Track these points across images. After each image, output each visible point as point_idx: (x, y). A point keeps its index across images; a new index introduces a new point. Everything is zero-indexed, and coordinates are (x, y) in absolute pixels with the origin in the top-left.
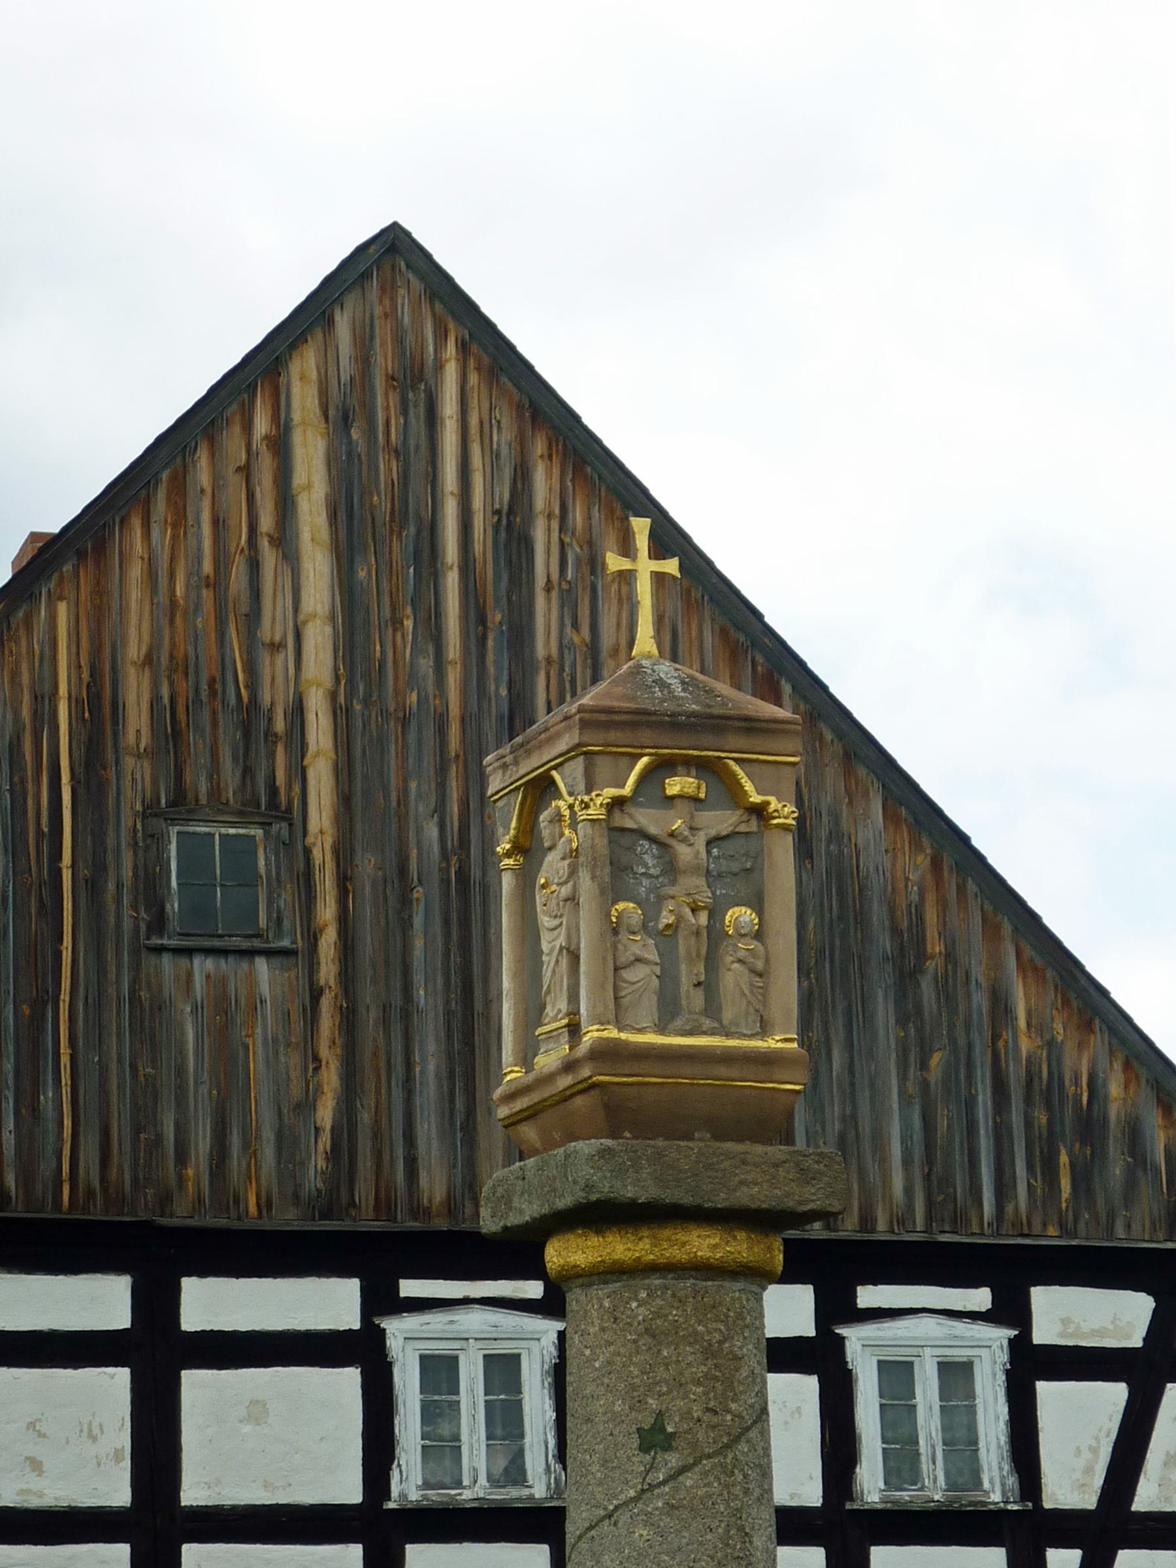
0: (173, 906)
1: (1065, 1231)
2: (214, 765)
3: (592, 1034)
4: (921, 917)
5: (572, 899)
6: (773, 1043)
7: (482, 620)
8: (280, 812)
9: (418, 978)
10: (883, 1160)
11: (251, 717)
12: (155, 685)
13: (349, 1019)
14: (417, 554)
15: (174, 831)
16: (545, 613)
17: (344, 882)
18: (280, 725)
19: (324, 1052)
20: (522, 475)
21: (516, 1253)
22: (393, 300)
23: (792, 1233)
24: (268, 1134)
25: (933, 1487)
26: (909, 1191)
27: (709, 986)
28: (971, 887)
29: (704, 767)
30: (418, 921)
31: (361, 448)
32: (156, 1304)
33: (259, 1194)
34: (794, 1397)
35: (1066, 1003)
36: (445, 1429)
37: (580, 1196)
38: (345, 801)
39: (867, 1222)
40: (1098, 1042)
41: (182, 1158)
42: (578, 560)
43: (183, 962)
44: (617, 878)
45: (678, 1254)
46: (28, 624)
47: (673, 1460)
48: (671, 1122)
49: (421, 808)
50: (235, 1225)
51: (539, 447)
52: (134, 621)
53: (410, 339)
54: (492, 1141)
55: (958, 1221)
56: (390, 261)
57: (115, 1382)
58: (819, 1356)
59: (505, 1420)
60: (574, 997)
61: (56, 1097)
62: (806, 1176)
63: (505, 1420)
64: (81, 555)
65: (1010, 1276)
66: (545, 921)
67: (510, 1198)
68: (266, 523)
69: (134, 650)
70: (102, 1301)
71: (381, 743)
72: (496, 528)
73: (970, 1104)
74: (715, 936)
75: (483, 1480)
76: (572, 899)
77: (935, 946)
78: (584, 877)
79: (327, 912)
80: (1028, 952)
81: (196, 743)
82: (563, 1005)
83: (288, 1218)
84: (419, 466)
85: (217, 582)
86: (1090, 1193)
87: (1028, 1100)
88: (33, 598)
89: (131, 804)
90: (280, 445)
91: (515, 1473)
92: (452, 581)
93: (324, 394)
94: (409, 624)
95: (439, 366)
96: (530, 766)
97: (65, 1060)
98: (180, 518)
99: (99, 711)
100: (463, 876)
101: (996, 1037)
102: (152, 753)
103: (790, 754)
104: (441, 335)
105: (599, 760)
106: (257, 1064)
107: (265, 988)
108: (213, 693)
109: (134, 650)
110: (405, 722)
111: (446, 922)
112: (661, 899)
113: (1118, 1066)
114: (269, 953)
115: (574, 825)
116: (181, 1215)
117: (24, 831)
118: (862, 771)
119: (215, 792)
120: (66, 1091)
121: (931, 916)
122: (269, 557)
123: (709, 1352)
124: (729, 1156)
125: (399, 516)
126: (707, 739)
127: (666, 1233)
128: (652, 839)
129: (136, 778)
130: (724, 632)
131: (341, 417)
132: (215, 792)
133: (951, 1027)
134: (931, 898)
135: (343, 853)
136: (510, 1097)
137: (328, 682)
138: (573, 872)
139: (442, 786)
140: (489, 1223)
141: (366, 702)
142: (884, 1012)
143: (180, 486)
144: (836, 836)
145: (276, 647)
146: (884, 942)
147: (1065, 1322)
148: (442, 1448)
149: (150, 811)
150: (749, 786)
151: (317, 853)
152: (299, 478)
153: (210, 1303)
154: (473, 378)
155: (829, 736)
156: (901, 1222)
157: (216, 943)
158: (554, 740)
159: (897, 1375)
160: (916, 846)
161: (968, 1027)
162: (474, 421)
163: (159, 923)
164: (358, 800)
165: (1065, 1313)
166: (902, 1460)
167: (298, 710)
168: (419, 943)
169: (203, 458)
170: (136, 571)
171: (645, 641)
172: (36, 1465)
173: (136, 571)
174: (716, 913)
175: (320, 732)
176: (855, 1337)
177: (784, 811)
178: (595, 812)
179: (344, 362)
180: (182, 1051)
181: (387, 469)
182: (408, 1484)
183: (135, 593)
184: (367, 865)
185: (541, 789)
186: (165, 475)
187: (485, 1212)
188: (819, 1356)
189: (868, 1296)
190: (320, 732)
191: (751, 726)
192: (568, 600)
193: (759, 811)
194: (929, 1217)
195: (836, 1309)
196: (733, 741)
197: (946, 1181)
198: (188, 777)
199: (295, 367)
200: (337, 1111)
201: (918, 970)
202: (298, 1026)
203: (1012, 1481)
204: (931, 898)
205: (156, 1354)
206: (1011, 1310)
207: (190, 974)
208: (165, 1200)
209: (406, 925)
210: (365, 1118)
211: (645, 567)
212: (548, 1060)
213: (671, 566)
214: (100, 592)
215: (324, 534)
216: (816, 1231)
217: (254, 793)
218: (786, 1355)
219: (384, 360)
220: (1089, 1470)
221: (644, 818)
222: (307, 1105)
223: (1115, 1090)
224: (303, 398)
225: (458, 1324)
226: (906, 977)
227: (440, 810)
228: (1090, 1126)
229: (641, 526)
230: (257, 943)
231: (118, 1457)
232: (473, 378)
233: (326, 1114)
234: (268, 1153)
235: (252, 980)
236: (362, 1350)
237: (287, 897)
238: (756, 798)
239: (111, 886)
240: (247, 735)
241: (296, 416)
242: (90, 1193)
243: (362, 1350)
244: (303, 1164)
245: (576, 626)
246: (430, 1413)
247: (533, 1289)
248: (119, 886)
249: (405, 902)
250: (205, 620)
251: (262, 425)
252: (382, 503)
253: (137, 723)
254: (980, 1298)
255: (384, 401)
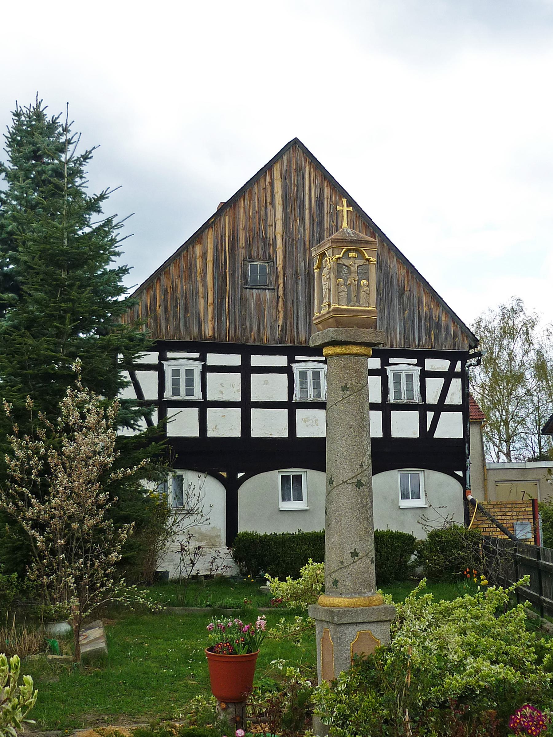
0: (249, 279)
1: (432, 348)
2: (258, 250)
3: (333, 306)
4: (404, 282)
5: (329, 278)
6: (370, 308)
7: (314, 220)
8: (271, 260)
9: (300, 294)
10: (395, 333)
11: (265, 240)
12: (246, 234)
13: (285, 303)
14: (300, 206)
15: (249, 264)
16: (326, 219)
17: (284, 274)
18: (271, 242)
19: (280, 310)
20: (322, 190)
21: (317, 351)
22: (295, 154)
23: (373, 348)
24: (269, 327)
25: (404, 399)
26: (400, 339)
27: (357, 296)
28: (414, 276)
29: (357, 251)
30: (300, 283)
31: (289, 184)
32: (246, 360)
33: (267, 339)
34: (375, 382)
35: (434, 300)
36: (304, 387)
37: (330, 340)
38: (285, 257)
39: (392, 345)
40: (440, 308)
41: (251, 331)
42: (333, 207)
43: (251, 290)
44: (338, 275)
45: (350, 351)
46: (220, 220)
47: (349, 393)
48: (348, 324)
49: (300, 259)
50: (262, 345)
51: (326, 184)
52: (241, 221)
53: (299, 162)
54: (314, 328)
55: (410, 346)
56: (295, 145)
57: (237, 377)
58: (381, 373)
59: (317, 385)
60: (329, 298)
61: (225, 318)
62: (377, 336)
63: (317, 385)
64: (231, 207)
65: (421, 356)
66: (324, 283)
67: (315, 341)
68: (269, 200)
69: (241, 226)
70: (235, 360)
71: (292, 246)
72: (316, 201)
73: (413, 321)
74: (359, 286)
75: (312, 397)
76: (329, 278)
77: (407, 289)
78: (332, 274)
79: (281, 281)
80: (426, 290)
81: (254, 247)
82: (327, 300)
83: (272, 344)
84: (300, 188)
85: (258, 212)
86: (438, 339)
87: (425, 320)
88: (221, 216)
89: (241, 259)
90: (272, 184)
91: (319, 395)
92: (307, 212)
93: (281, 173)
94: (298, 221)
95: (305, 167)
96: (321, 250)
97: (227, 311)
98: (251, 199)
99: (234, 239)
100: (309, 273)
101: (419, 308)
102: (245, 248)
103: (376, 248)
104: (305, 161)
105: (335, 249)
106: (266, 312)
107: (268, 297)
108: (258, 235)
109: (241, 226)
110: (297, 242)
111: (305, 283)
112: (348, 278)
113: (444, 314)
114: (269, 289)
115: (330, 263)
116: (251, 343)
117: (219, 263)
118: (392, 252)
119: (258, 256)
120: (227, 317)
121: (406, 282)
122: (269, 207)
123: (356, 371)
124: (361, 331)
125: (296, 198)
126: (358, 245)
127: (348, 347)
128: (346, 266)
129: (242, 253)
130: (364, 223)
131: (285, 178)
132: (258, 256)
133: (410, 305)
134: (406, 279)
135: (284, 269)
136: (316, 319)
137: (281, 233)
138: (329, 272)
139: (305, 255)
140: (311, 345)
141: (289, 237)
142: (396, 302)
143: (251, 192)
144: (387, 266)
145: (271, 226)
146: (397, 288)
147: (432, 366)
148: (304, 390)
149: (245, 260)
150: (366, 255)
151: (279, 268)
152: (276, 191)
153: (256, 360)
154: (312, 170)
155: (385, 245)
156: (399, 345)
157: (258, 287)
158: (326, 245)
159: (397, 377)
160: (403, 268)
161: (413, 305)
162: (312, 179)
163: (246, 283)
164: (287, 258)
165: (431, 364)
166: (398, 393)
167: (275, 239)
168: (300, 287)
169: (256, 186)
170: (242, 210)
171: (345, 225)
172: (222, 392)
173: (242, 210)
174: (359, 281)
175: (279, 243)
176: (388, 368)
177: (374, 260)
178: (334, 260)
179: (285, 166)
180: (251, 308)
181: (294, 189)
182: (297, 397)
183: (242, 214)
184: (289, 271)
185: (323, 255)
186: (248, 190)
187: (310, 342)
188: (381, 373)
189: (392, 360)
190: (279, 243)
191: (367, 242)
192: (331, 216)
193: (368, 260)
194: (404, 345)
195: (385, 363)
196: (363, 246)
197: (409, 336)
198: (252, 253)
199: (275, 167)
200: (283, 322)
201: (404, 293)
202: (275, 304)
203: (420, 398)
204: (406, 279)
205: (246, 371)
206: (421, 364)
207: (253, 293)
208: (248, 339)
209: (297, 283)
210: (288, 323)
211: (345, 209)
212: (324, 312)
213: (351, 209)
214: (234, 215)
215: (281, 202)
216: (381, 347)
217: (266, 256)
218: (373, 372)
219: (293, 166)
220: (436, 396)
221: (345, 261)
222: (277, 321)
223: (443, 319)
224: (277, 174)
225: (306, 365)
226: (401, 295)
227: (304, 260)
228: (438, 326)
229: (345, 200)
230: (266, 287)
231: (238, 391)
232: (312, 170)
233: (280, 322)
234: (269, 330)
235: (265, 295)
236: (288, 370)
237: (272, 278)
238: (368, 258)
239: (237, 275)
240: (264, 244)
241: (275, 178)
242: (232, 338)
243: (288, 370)
244: (276, 333)
245: (333, 222)
246: (301, 383)
247: (323, 359)
248: (238, 275)
249: (297, 279)
250: (256, 220)
251: (268, 180)
252: (293, 196)
253: (242, 242)
254: (415, 361)
255: (293, 174)
